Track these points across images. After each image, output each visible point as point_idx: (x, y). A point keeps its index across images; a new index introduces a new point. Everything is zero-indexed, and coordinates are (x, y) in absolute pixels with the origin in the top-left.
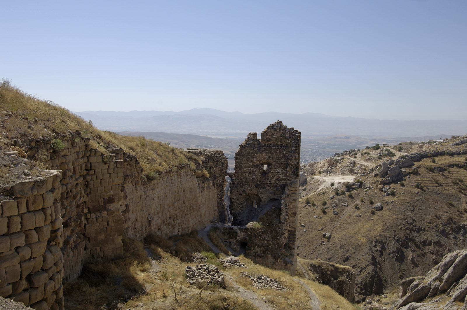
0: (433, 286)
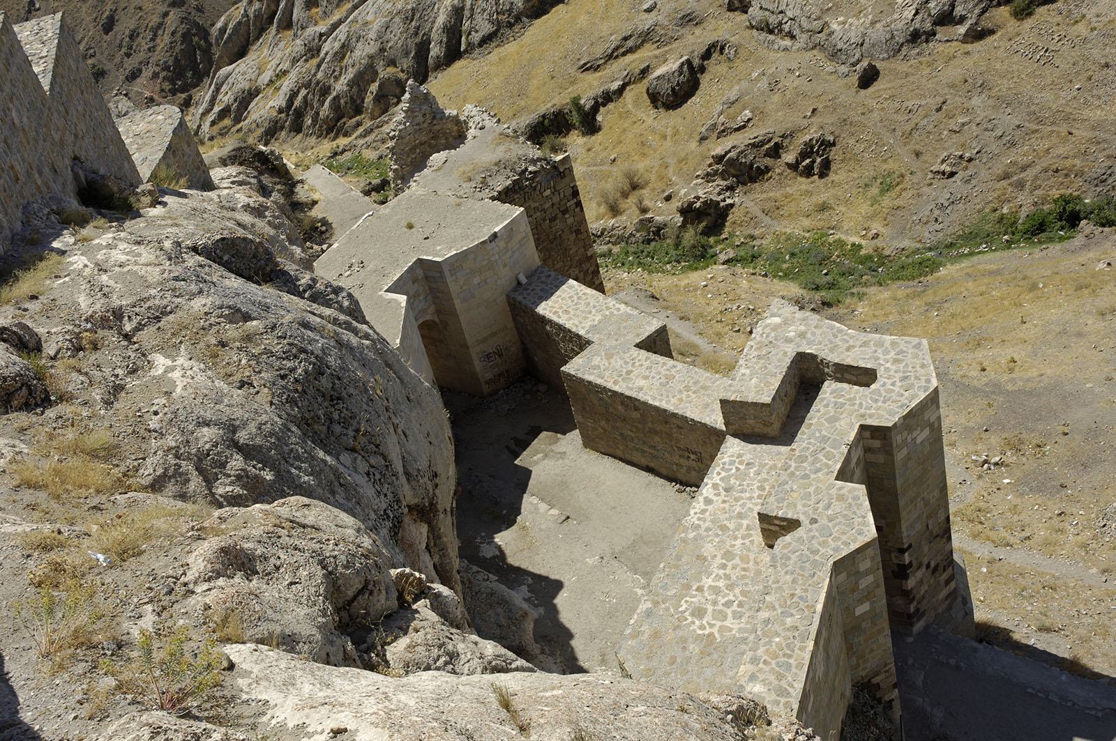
0: (252, 16)
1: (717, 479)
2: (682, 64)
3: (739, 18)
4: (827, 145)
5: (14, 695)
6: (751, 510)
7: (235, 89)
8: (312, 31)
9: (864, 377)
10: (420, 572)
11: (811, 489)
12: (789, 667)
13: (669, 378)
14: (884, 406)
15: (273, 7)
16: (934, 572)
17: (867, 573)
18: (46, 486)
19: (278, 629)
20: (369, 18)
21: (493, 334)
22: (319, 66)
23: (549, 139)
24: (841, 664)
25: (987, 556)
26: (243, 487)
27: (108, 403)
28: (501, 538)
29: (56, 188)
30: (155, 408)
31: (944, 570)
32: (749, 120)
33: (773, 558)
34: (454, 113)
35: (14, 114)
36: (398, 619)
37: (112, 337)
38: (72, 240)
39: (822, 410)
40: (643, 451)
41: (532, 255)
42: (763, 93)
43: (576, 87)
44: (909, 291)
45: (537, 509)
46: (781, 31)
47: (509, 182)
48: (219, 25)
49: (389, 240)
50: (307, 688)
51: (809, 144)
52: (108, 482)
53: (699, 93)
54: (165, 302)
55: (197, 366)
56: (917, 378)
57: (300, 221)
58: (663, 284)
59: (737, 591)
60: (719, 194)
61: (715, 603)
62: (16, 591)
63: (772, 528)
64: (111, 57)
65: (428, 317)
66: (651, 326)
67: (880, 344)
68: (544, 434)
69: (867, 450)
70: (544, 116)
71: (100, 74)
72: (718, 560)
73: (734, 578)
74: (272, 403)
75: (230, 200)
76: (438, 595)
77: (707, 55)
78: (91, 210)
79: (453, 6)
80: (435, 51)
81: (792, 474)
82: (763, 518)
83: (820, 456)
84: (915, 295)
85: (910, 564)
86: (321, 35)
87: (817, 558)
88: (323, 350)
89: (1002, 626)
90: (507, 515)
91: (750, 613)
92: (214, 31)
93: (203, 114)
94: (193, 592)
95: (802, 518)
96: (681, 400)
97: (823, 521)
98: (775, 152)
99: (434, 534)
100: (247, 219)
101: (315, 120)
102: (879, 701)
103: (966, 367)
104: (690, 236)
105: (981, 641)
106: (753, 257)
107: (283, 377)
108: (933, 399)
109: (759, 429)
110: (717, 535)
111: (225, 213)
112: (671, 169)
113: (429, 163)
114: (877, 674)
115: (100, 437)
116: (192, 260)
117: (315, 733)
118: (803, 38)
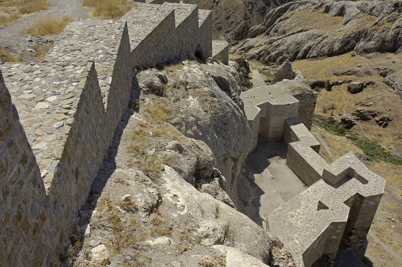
1: (313, 188)
2: (361, 83)
3: (382, 78)
4: (389, 120)
5: (117, 153)
6: (318, 199)
7: (248, 44)
8: (273, 38)
9: (365, 182)
10: (220, 171)
11: (336, 202)
12: (307, 241)
13: (315, 158)
14: (366, 191)
15: (266, 29)
16: (359, 238)
17: (340, 229)
18: (151, 113)
19: (179, 168)
20: (288, 40)
21: (277, 127)
22: (270, 47)
23: (317, 88)
24: (322, 247)
25: (377, 242)
26: (194, 134)
27: (174, 102)
28: (256, 175)
29: (191, 50)
30: (183, 107)
31: (362, 239)
32: (371, 105)
33: (317, 213)
34: (295, 71)
35: (189, 29)
36: (209, 179)
37: (183, 88)
38: (187, 63)
39: (349, 184)
40: (300, 172)
41: (296, 113)
42: (378, 100)
43: (330, 78)
44: (392, 166)
45: (267, 173)
46: (391, 86)
47: (299, 93)
48: (252, 28)
49: (262, 95)
50: (177, 183)
51: (384, 118)
52: (165, 118)
53: (361, 92)
54: (199, 85)
55: (198, 102)
56: (378, 188)
57: (246, 81)
58: (328, 135)
59: (304, 216)
60: (354, 120)
61: (297, 216)
62: (130, 132)
63: (321, 206)
64: (225, 26)
65: (264, 116)
66: (317, 143)
67: (373, 175)
68: (278, 156)
69: (356, 200)
70: (318, 81)
71: (220, 29)
72: (304, 207)
73: (305, 213)
74: (210, 118)
75: (229, 70)
76: (222, 179)
77: (368, 84)
78: (196, 58)
79: (309, 46)
80: (300, 55)
81: (333, 196)
82: (320, 202)
83: (342, 195)
84: (393, 168)
85: (353, 233)
86: (274, 40)
87: (328, 219)
88: (228, 112)
89: (371, 261)
90: (260, 171)
91: (305, 223)
92: (250, 29)
93: (239, 47)
94: (166, 150)
95: (329, 207)
96: (315, 165)
97: (334, 211)
98: (374, 116)
99: (235, 166)
100: (230, 75)
101: (263, 59)
102: (328, 262)
103: (397, 193)
104: (341, 127)
105: (363, 262)
106: (355, 139)
107: (216, 114)
108: (380, 196)
109: (330, 181)
110: (306, 201)
111: (226, 72)
112: (344, 108)
113: (283, 80)
114: (330, 255)
115: (168, 108)
116: (210, 79)
117: (171, 193)
118: (396, 90)
